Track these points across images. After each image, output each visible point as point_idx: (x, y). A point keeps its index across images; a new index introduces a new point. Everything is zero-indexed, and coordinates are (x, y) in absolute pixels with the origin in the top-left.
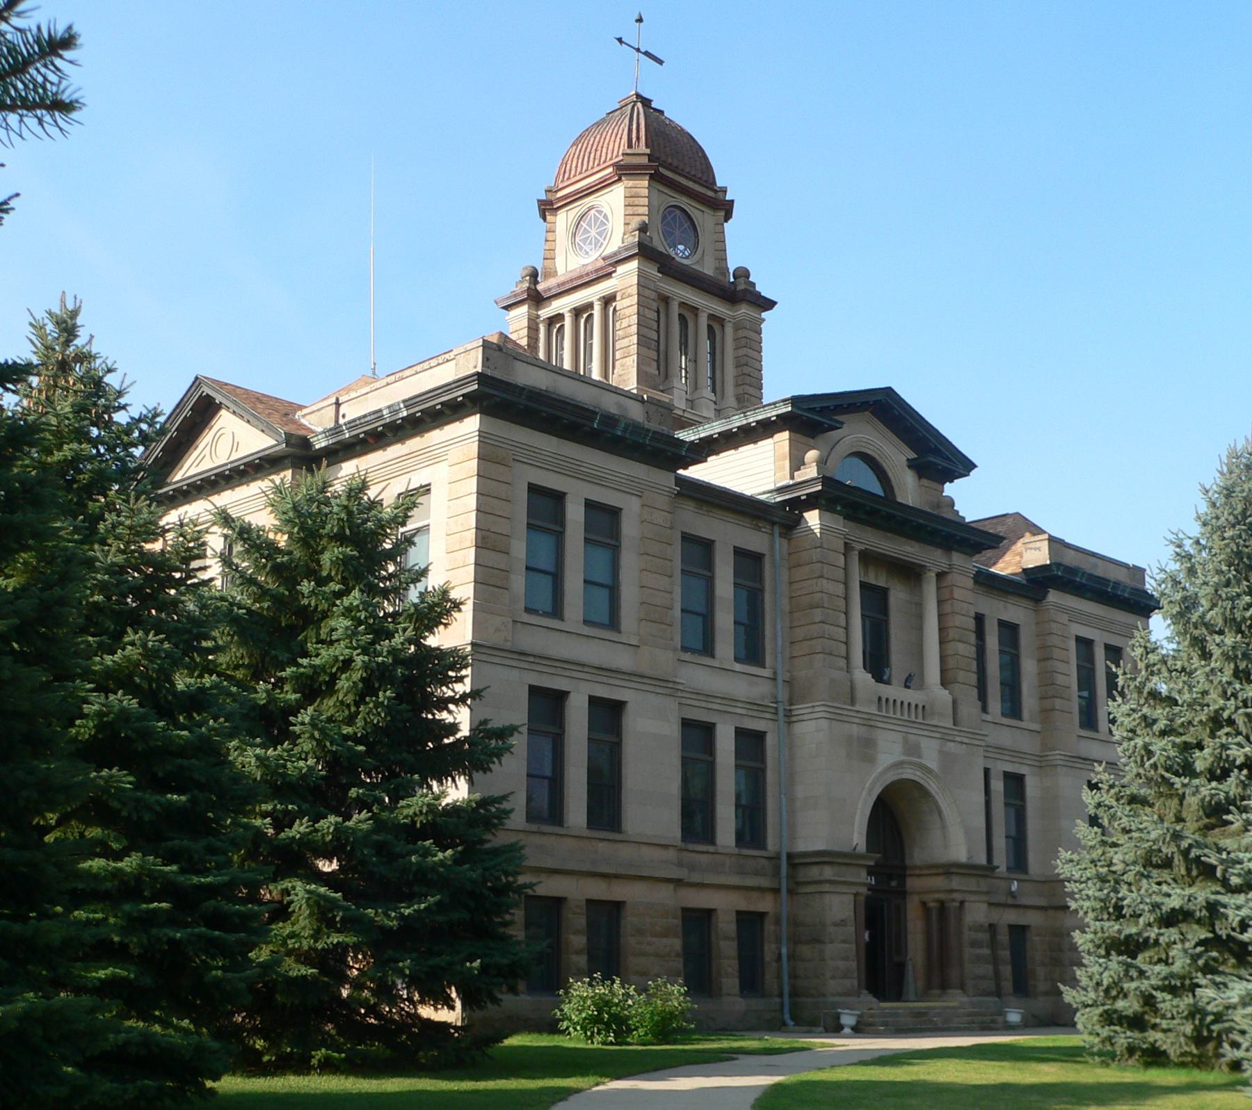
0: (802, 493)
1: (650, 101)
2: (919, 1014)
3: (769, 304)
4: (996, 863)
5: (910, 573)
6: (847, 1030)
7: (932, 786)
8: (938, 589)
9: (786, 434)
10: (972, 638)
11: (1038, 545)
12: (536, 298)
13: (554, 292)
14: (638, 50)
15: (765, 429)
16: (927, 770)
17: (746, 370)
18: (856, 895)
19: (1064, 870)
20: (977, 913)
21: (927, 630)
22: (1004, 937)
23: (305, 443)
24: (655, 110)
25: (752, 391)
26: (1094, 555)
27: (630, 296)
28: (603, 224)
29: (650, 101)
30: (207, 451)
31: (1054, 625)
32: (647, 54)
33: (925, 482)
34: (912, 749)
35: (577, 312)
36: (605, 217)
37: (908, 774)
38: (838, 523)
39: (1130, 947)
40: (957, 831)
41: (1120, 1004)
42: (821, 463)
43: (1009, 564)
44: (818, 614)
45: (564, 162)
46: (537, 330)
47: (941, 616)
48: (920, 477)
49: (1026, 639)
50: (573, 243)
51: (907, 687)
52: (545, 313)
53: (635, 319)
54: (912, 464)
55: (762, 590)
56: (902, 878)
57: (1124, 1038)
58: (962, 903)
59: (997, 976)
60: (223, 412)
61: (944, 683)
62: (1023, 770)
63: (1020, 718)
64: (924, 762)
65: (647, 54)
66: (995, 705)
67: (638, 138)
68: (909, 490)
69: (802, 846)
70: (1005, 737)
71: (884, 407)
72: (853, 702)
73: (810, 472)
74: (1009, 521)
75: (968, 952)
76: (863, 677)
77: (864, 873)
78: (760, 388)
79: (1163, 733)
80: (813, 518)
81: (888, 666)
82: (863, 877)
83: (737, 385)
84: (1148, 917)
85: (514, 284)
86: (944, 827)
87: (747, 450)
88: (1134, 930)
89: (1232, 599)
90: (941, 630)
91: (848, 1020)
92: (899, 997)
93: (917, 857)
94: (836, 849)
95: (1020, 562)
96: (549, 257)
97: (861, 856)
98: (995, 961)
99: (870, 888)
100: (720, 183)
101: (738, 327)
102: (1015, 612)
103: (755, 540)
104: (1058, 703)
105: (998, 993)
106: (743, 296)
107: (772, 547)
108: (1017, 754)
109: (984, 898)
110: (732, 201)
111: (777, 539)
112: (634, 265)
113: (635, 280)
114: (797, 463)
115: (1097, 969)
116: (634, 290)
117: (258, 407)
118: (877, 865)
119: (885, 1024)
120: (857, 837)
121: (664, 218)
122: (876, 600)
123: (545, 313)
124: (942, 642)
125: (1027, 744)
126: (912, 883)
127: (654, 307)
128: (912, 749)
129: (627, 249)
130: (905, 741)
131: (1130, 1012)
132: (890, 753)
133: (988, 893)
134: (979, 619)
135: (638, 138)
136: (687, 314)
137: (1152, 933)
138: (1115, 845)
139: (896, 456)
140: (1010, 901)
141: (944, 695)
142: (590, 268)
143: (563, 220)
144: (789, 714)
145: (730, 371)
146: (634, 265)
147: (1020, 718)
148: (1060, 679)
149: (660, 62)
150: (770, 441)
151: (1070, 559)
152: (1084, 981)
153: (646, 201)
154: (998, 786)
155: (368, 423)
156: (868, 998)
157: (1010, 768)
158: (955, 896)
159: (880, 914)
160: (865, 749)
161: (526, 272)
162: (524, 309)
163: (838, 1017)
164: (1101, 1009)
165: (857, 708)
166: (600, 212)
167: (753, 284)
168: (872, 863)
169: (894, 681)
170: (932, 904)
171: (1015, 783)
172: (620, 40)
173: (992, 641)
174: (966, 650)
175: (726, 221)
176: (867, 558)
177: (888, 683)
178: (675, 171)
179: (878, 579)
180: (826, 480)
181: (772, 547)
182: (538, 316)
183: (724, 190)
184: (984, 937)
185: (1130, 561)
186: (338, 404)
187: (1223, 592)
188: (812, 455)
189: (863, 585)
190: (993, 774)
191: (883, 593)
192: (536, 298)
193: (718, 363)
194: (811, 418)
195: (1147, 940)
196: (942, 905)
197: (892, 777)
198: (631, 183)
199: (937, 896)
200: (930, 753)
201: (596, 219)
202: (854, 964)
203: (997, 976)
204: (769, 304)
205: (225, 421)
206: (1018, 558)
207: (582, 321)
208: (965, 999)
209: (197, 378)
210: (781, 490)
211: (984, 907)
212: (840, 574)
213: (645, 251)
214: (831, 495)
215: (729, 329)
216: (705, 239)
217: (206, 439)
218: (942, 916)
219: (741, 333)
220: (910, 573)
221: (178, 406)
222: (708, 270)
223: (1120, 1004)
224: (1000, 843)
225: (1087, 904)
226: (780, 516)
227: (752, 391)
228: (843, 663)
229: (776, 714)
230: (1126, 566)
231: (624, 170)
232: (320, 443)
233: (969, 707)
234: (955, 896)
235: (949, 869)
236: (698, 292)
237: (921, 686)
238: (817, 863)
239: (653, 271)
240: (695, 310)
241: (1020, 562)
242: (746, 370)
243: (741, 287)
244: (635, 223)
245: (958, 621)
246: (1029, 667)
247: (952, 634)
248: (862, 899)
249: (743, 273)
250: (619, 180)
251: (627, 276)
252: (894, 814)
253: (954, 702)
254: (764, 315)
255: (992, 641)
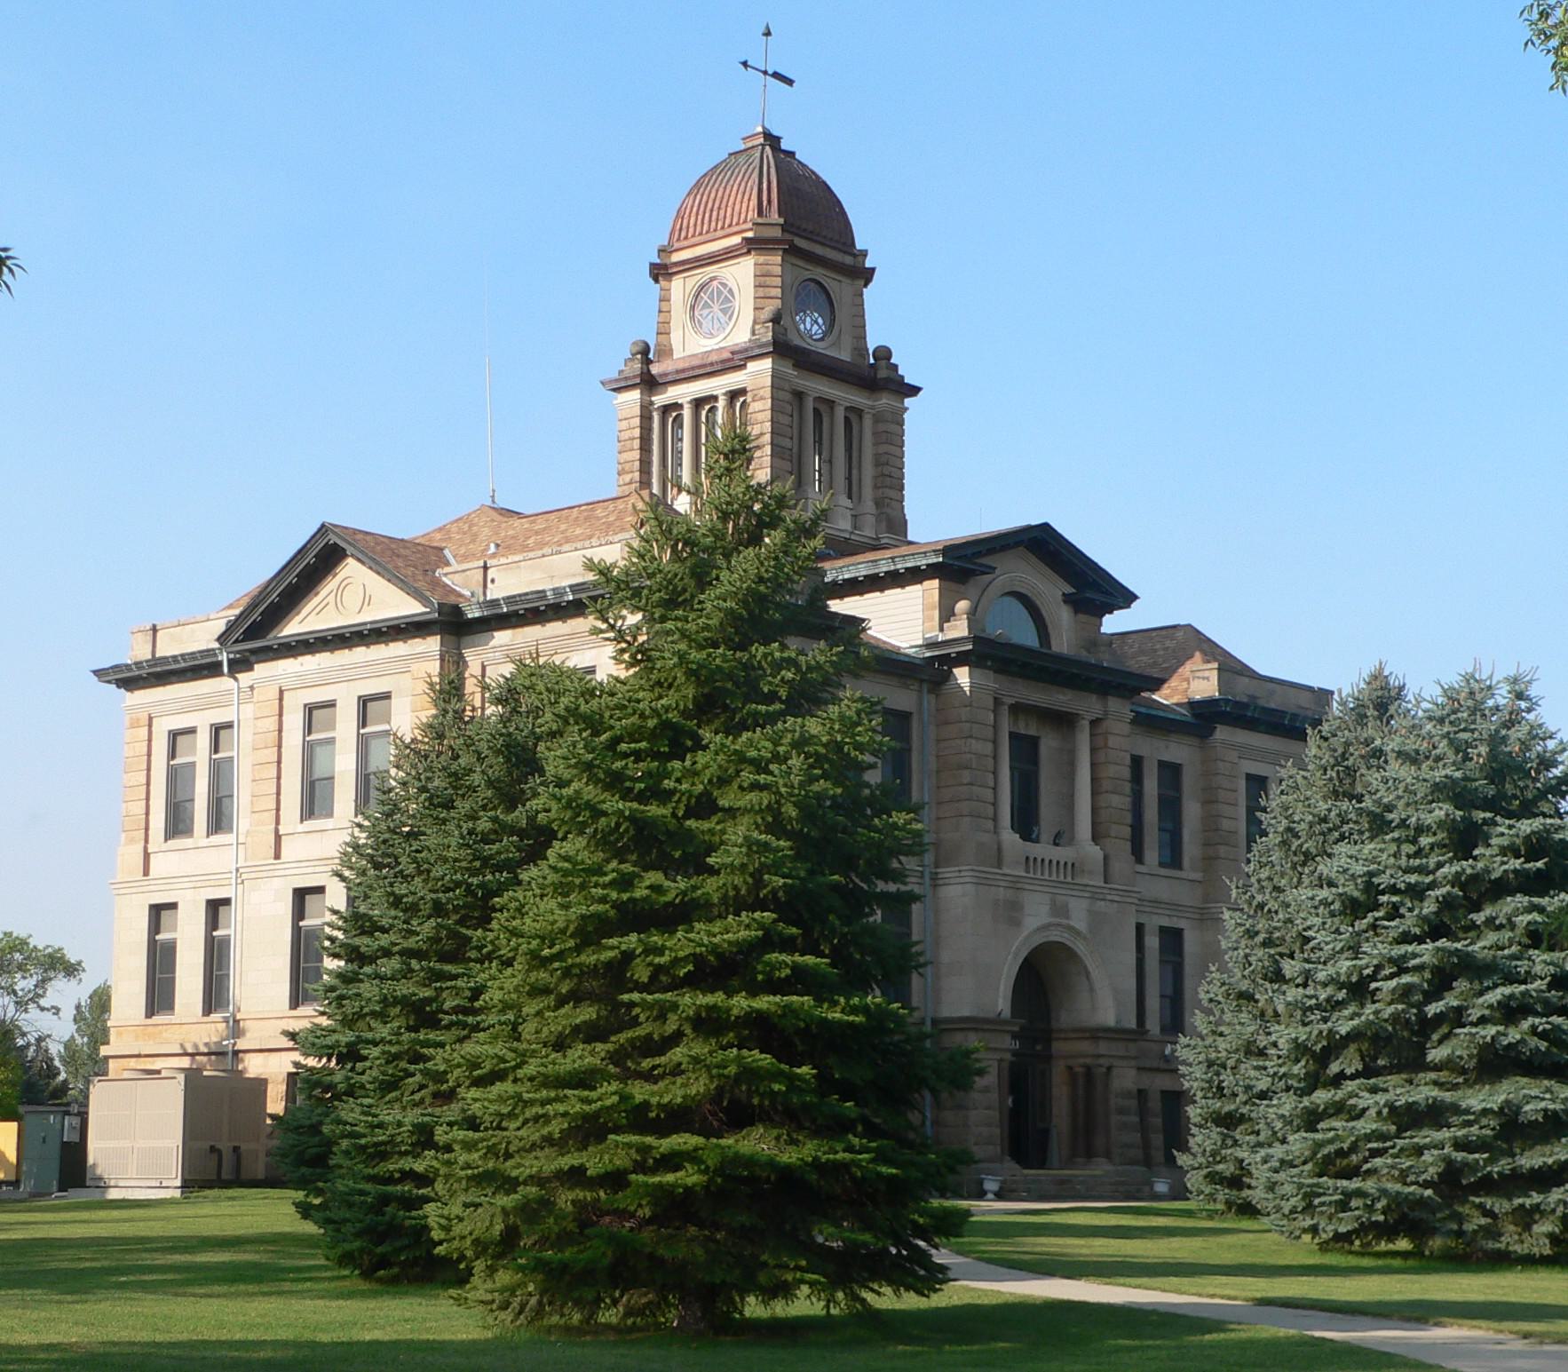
0: (953, 650)
1: (778, 139)
2: (1062, 1182)
3: (914, 390)
4: (1148, 1026)
5: (1063, 721)
6: (990, 1196)
7: (1080, 948)
8: (1091, 735)
9: (936, 583)
10: (1127, 787)
11: (1206, 674)
12: (650, 383)
13: (670, 378)
14: (765, 73)
15: (914, 576)
16: (1077, 933)
17: (887, 470)
18: (1001, 1061)
19: (1182, 1053)
20: (1126, 1079)
21: (1080, 786)
22: (1155, 1104)
23: (457, 610)
24: (785, 152)
25: (892, 493)
26: (1272, 680)
27: (762, 398)
28: (727, 300)
29: (778, 139)
30: (331, 599)
31: (1221, 764)
32: (776, 75)
33: (1082, 617)
34: (1060, 910)
35: (698, 403)
36: (731, 291)
37: (1055, 936)
38: (990, 681)
39: (1229, 1121)
40: (1105, 995)
41: (1220, 1167)
42: (972, 615)
43: (1175, 690)
44: (966, 776)
45: (680, 215)
46: (650, 418)
47: (1093, 765)
48: (1076, 612)
49: (1190, 782)
50: (692, 318)
51: (1056, 844)
52: (660, 400)
53: (768, 426)
54: (1067, 599)
55: (910, 750)
56: (1048, 1041)
57: (1223, 1194)
58: (1109, 1069)
59: (1146, 1145)
60: (350, 560)
61: (1096, 837)
62: (1181, 924)
63: (1179, 866)
64: (1072, 923)
65: (776, 75)
66: (1152, 855)
67: (769, 202)
68: (1065, 636)
69: (946, 1012)
70: (1162, 887)
71: (1042, 544)
72: (999, 865)
73: (959, 629)
74: (1180, 634)
75: (1115, 1119)
76: (1010, 837)
77: (1008, 1038)
78: (902, 488)
79: (1265, 944)
80: (962, 676)
81: (1037, 823)
82: (1008, 1043)
83: (876, 487)
84: (1242, 1097)
85: (618, 361)
86: (1092, 990)
87: (894, 594)
88: (1233, 1107)
89: (1323, 833)
90: (1094, 780)
91: (991, 1185)
92: (1042, 1164)
93: (1064, 1019)
94: (981, 1015)
95: (1186, 690)
96: (663, 330)
97: (1005, 1022)
98: (1144, 1128)
99: (1015, 1053)
100: (859, 245)
101: (878, 419)
102: (1177, 750)
103: (901, 698)
104: (1222, 850)
105: (1148, 1162)
106: (883, 381)
107: (920, 704)
108: (1174, 907)
109: (1133, 1063)
110: (873, 270)
111: (926, 697)
112: (767, 363)
113: (768, 382)
114: (947, 615)
115: (1203, 1139)
116: (767, 393)
117: (390, 558)
118: (1022, 1028)
119: (1028, 1191)
120: (1002, 1002)
121: (798, 295)
122: (1025, 752)
123: (660, 400)
124: (1095, 793)
125: (1186, 896)
126: (1058, 1047)
127: (787, 400)
128: (1060, 910)
129: (760, 347)
130: (1053, 903)
131: (1228, 1174)
132: (1036, 919)
133: (1135, 1058)
134: (1137, 762)
135: (769, 202)
136: (823, 408)
137: (1244, 1110)
138: (1221, 1035)
139: (1050, 590)
140: (1163, 1065)
141: (1095, 852)
142: (714, 358)
143: (680, 288)
144: (935, 877)
145: (868, 471)
146: (767, 363)
147: (1179, 866)
148: (1226, 824)
149: (790, 82)
150: (918, 587)
151: (1243, 689)
152: (1195, 1149)
153: (778, 281)
154: (1152, 942)
155: (529, 601)
156: (1010, 1166)
157: (1166, 922)
158: (1101, 1061)
159: (1024, 1082)
160: (1011, 913)
161: (636, 349)
162: (635, 395)
163: (981, 1182)
164: (1205, 1171)
165: (1006, 871)
166: (725, 285)
167: (895, 367)
168: (1016, 1029)
169: (1044, 837)
170: (1080, 1070)
171: (1172, 939)
172: (745, 64)
173: (1151, 786)
174: (1119, 801)
175: (866, 285)
176: (1017, 709)
177: (1037, 841)
178: (809, 233)
179: (1029, 728)
180: (977, 639)
181: (920, 704)
182: (652, 403)
183: (864, 254)
184: (1133, 1103)
185: (1315, 684)
186: (485, 568)
187: (1317, 829)
188: (962, 605)
189: (1012, 735)
190: (1147, 929)
191: (1034, 742)
192: (650, 383)
193: (855, 454)
194: (961, 565)
195: (1242, 1115)
196: (1089, 1070)
197: (1038, 940)
198: (762, 259)
199: (1082, 1061)
200: (1079, 920)
201: (720, 293)
202: (998, 1131)
203: (1146, 1145)
204: (914, 390)
205: (351, 569)
206: (1185, 685)
207: (704, 413)
208: (1110, 1168)
209: (323, 526)
210: (930, 645)
211: (1133, 1072)
212: (989, 733)
213: (783, 348)
214: (984, 652)
215: (868, 421)
216: (842, 315)
217: (329, 587)
218: (1089, 1082)
219: (882, 427)
220: (1063, 721)
221: (300, 551)
222: (845, 355)
223: (1220, 1167)
224: (1153, 1003)
225: (1195, 1084)
226: (928, 671)
227: (892, 493)
228: (990, 824)
229: (922, 877)
230: (1310, 689)
231: (753, 245)
232: (473, 613)
233: (1122, 862)
234: (1101, 1061)
235: (1098, 1034)
236: (842, 395)
237: (1072, 840)
238: (962, 1029)
239: (789, 370)
240: (831, 404)
241: (1186, 690)
242: (887, 470)
243: (882, 374)
244: (767, 313)
245: (1112, 771)
246: (1192, 811)
247: (1106, 785)
248: (1006, 1065)
249: (884, 354)
250: (749, 252)
251: (760, 372)
252: (1042, 977)
253: (1106, 858)
254: (908, 402)
255: (1151, 786)
